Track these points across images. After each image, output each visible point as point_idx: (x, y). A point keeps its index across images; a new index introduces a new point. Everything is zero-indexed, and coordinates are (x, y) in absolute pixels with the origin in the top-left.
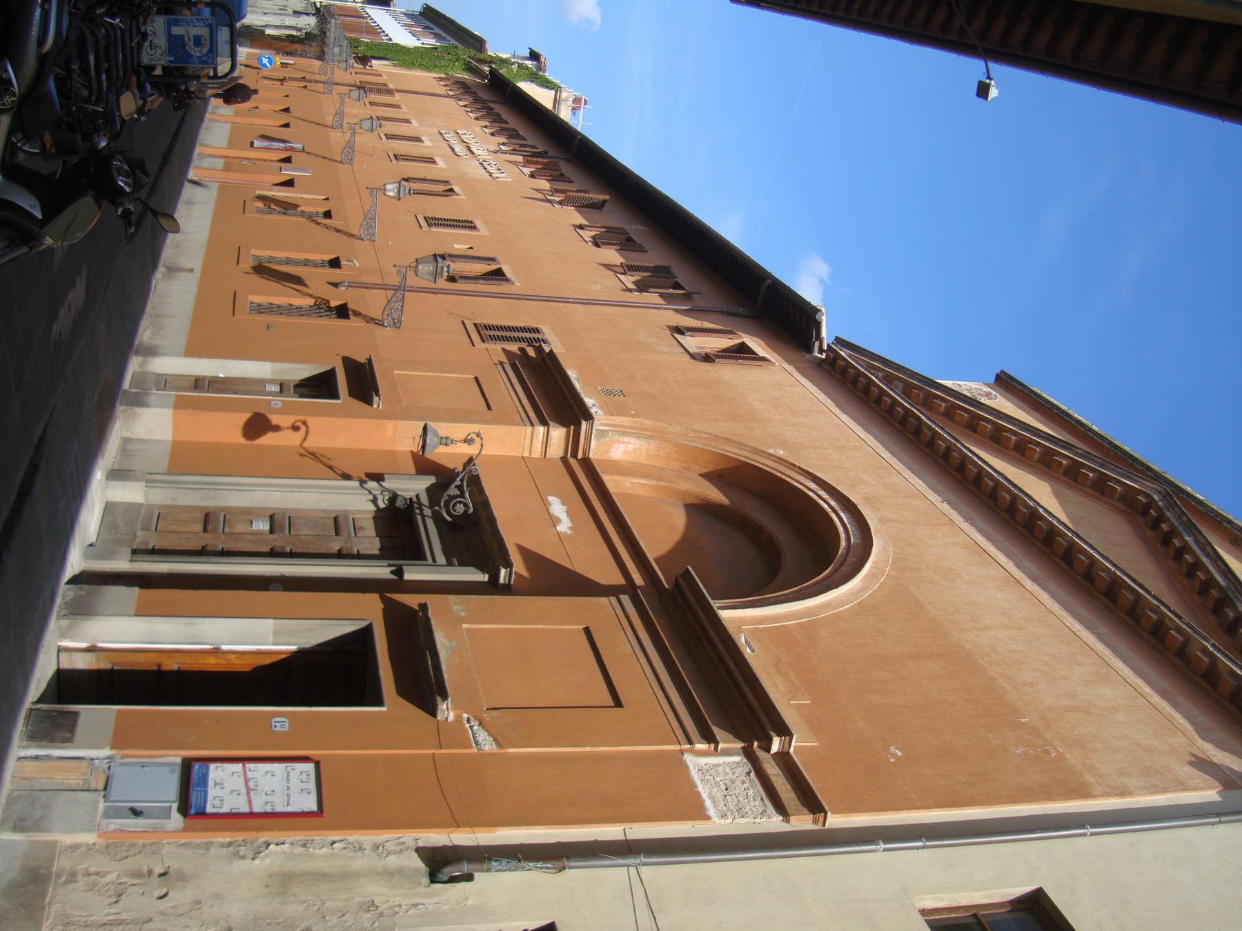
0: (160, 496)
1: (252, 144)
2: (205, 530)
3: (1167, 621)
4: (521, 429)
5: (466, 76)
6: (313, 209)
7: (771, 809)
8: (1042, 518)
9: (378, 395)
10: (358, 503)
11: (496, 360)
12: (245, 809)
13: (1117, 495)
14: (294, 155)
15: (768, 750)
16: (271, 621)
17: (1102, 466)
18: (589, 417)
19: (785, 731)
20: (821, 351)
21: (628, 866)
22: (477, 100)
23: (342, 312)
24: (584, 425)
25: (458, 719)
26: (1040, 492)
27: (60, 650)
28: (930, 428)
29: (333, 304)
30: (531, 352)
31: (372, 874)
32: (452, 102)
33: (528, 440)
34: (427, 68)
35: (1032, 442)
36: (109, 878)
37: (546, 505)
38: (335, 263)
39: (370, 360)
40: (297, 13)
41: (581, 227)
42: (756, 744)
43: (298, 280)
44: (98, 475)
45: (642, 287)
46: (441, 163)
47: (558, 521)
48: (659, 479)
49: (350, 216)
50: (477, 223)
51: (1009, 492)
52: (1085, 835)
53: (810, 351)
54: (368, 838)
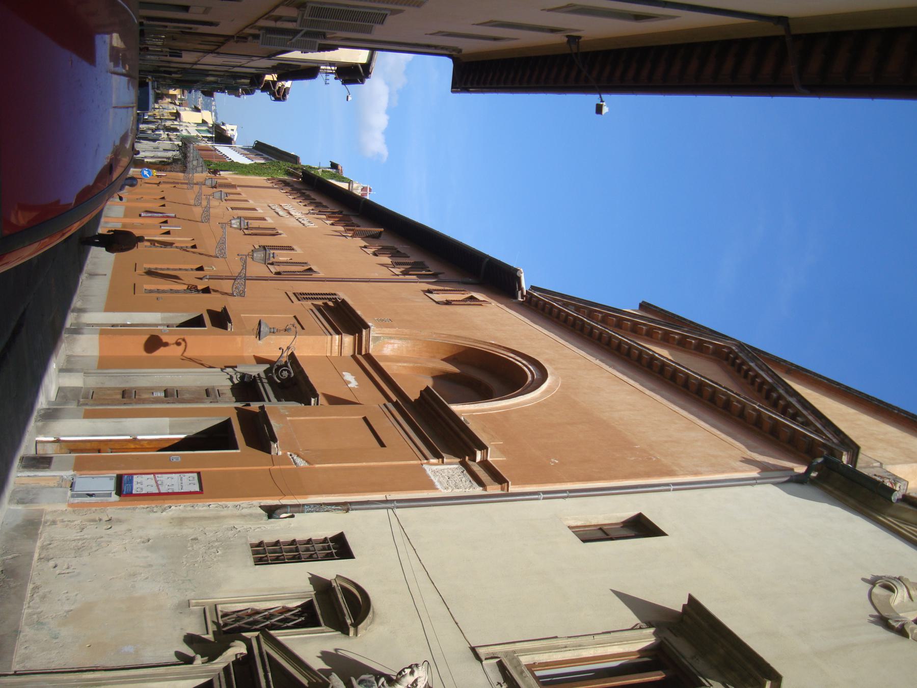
0: (93, 382)
1: (140, 215)
2: (123, 397)
3: (732, 399)
4: (323, 337)
5: (286, 177)
6: (184, 245)
7: (475, 484)
8: (657, 359)
9: (230, 322)
10: (222, 381)
11: (307, 308)
12: (157, 491)
13: (710, 352)
14: (169, 220)
15: (474, 460)
16: (167, 419)
17: (700, 335)
18: (367, 327)
19: (483, 447)
20: (523, 296)
21: (387, 508)
22: (294, 189)
23: (207, 290)
24: (364, 332)
25: (285, 454)
26: (663, 353)
27: (37, 442)
28: (589, 324)
29: (200, 288)
30: (331, 304)
31: (233, 517)
32: (277, 191)
33: (329, 345)
34: (259, 174)
35: (656, 328)
36: (76, 522)
37: (342, 377)
38: (201, 269)
39: (225, 309)
40: (165, 150)
41: (365, 247)
42: (467, 458)
43: (176, 277)
44: (53, 366)
45: (405, 273)
46: (269, 220)
47: (350, 382)
48: (415, 363)
49: (209, 245)
50: (295, 247)
51: (637, 349)
52: (669, 490)
53: (516, 297)
54: (230, 503)
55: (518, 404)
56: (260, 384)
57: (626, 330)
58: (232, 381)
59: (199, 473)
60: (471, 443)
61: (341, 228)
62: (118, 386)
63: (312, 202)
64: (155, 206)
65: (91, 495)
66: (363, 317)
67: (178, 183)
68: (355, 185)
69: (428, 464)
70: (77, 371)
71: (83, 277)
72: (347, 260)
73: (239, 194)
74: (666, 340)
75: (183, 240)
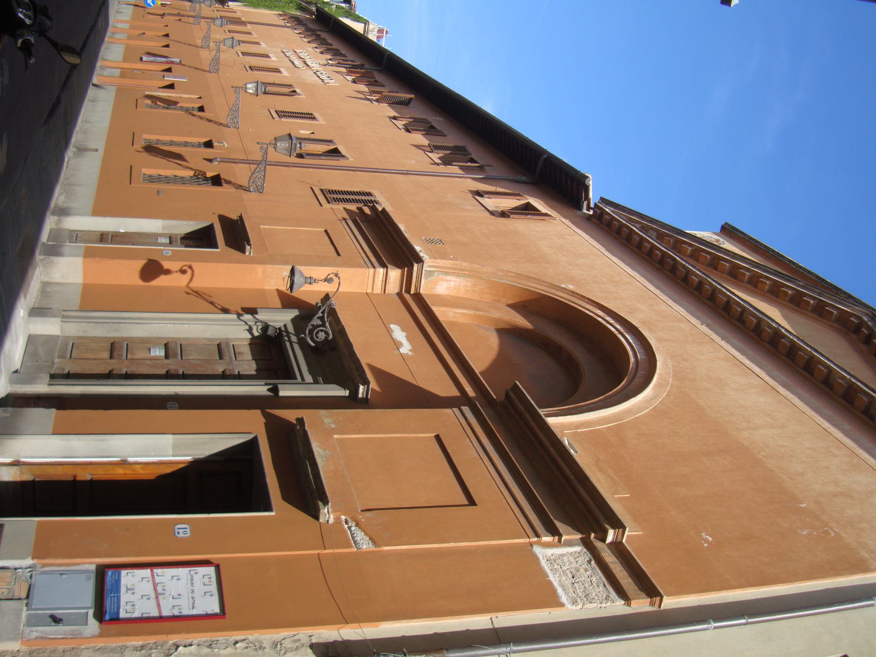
1: (141, 59)
2: (111, 357)
3: (705, 282)
5: (298, 13)
6: (190, 105)
7: (613, 594)
8: (784, 336)
9: (249, 244)
10: (237, 332)
11: (340, 216)
12: (155, 613)
13: (833, 318)
15: (603, 540)
17: (820, 294)
18: (420, 260)
19: (618, 524)
20: (589, 208)
22: (308, 29)
23: (217, 181)
26: (773, 312)
29: (209, 174)
30: (367, 210)
32: (290, 30)
33: (371, 279)
35: (762, 276)
37: (389, 332)
38: (209, 144)
39: (241, 217)
41: (395, 118)
42: (593, 535)
43: (179, 157)
45: (446, 161)
46: (285, 73)
48: (477, 309)
49: (219, 109)
50: (316, 115)
53: (580, 208)
55: (629, 412)
56: (288, 344)
57: (723, 272)
58: (251, 333)
59: (217, 567)
60: (602, 519)
61: (363, 88)
62: (105, 335)
63: (329, 50)
64: (156, 45)
65: (56, 620)
66: (410, 240)
67: (183, 16)
68: (371, 27)
69: (540, 544)
70: (54, 316)
71: (70, 153)
72: (430, 193)
73: (250, 33)
74: (775, 294)
75: (186, 97)
